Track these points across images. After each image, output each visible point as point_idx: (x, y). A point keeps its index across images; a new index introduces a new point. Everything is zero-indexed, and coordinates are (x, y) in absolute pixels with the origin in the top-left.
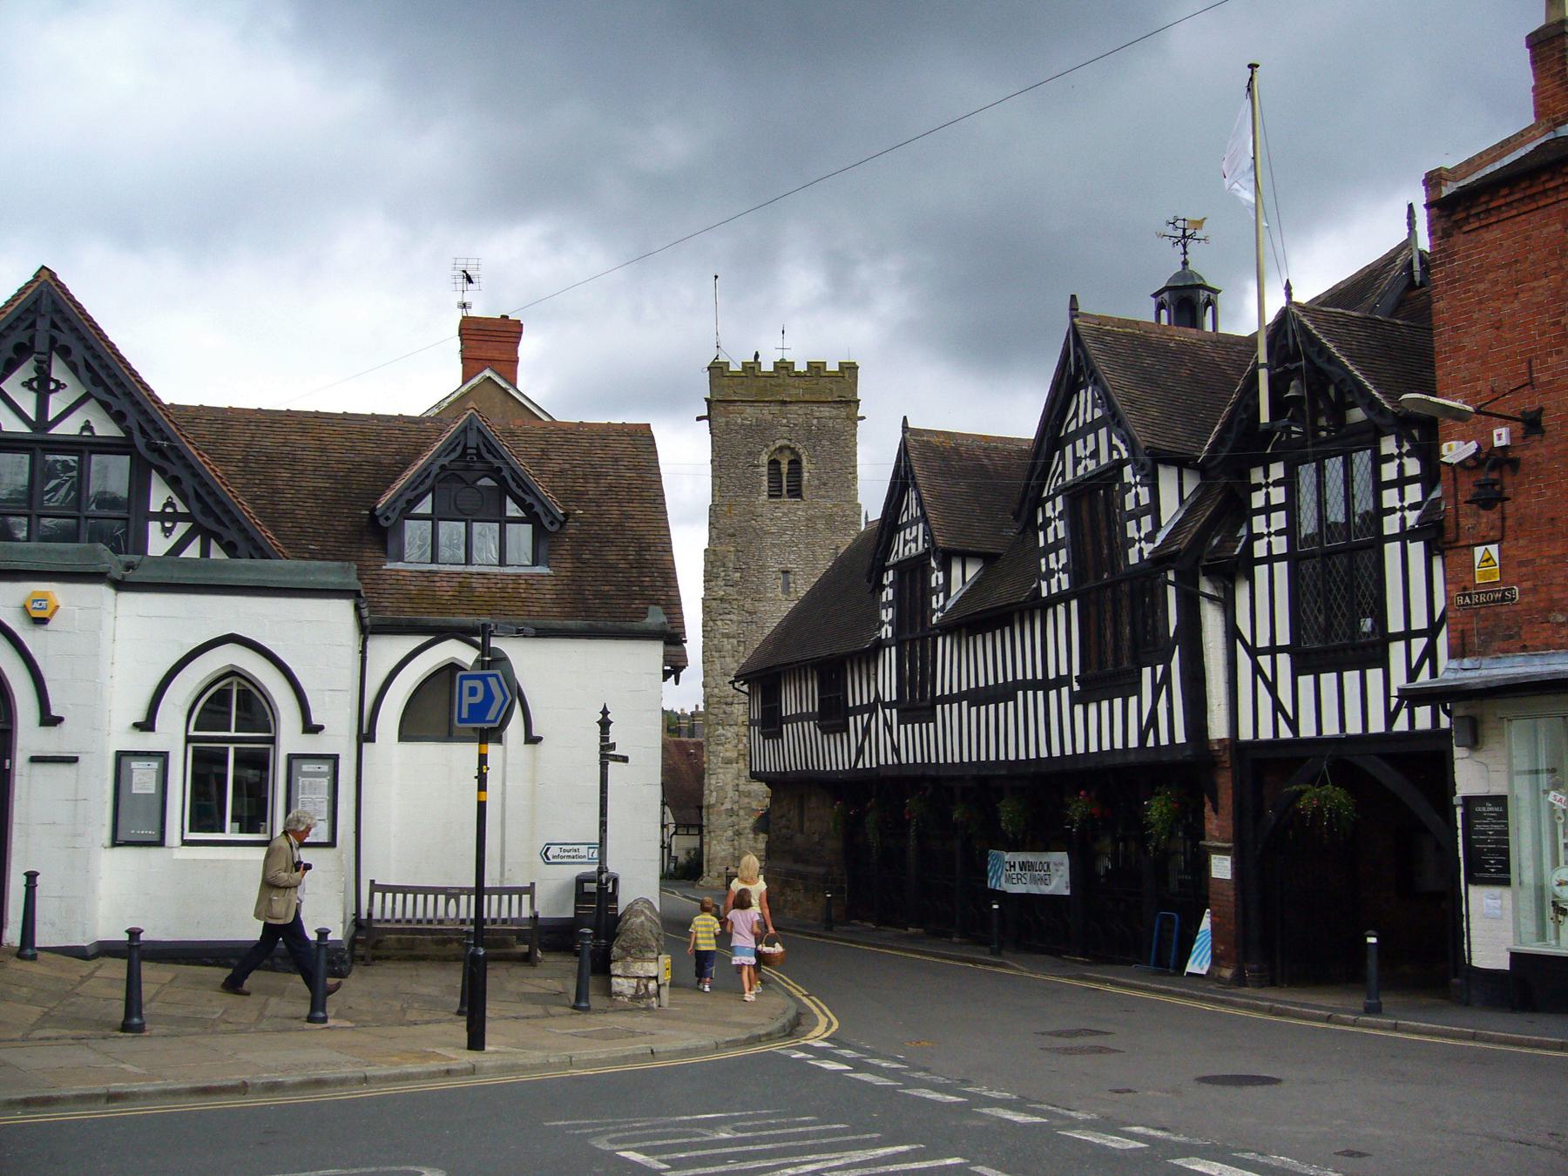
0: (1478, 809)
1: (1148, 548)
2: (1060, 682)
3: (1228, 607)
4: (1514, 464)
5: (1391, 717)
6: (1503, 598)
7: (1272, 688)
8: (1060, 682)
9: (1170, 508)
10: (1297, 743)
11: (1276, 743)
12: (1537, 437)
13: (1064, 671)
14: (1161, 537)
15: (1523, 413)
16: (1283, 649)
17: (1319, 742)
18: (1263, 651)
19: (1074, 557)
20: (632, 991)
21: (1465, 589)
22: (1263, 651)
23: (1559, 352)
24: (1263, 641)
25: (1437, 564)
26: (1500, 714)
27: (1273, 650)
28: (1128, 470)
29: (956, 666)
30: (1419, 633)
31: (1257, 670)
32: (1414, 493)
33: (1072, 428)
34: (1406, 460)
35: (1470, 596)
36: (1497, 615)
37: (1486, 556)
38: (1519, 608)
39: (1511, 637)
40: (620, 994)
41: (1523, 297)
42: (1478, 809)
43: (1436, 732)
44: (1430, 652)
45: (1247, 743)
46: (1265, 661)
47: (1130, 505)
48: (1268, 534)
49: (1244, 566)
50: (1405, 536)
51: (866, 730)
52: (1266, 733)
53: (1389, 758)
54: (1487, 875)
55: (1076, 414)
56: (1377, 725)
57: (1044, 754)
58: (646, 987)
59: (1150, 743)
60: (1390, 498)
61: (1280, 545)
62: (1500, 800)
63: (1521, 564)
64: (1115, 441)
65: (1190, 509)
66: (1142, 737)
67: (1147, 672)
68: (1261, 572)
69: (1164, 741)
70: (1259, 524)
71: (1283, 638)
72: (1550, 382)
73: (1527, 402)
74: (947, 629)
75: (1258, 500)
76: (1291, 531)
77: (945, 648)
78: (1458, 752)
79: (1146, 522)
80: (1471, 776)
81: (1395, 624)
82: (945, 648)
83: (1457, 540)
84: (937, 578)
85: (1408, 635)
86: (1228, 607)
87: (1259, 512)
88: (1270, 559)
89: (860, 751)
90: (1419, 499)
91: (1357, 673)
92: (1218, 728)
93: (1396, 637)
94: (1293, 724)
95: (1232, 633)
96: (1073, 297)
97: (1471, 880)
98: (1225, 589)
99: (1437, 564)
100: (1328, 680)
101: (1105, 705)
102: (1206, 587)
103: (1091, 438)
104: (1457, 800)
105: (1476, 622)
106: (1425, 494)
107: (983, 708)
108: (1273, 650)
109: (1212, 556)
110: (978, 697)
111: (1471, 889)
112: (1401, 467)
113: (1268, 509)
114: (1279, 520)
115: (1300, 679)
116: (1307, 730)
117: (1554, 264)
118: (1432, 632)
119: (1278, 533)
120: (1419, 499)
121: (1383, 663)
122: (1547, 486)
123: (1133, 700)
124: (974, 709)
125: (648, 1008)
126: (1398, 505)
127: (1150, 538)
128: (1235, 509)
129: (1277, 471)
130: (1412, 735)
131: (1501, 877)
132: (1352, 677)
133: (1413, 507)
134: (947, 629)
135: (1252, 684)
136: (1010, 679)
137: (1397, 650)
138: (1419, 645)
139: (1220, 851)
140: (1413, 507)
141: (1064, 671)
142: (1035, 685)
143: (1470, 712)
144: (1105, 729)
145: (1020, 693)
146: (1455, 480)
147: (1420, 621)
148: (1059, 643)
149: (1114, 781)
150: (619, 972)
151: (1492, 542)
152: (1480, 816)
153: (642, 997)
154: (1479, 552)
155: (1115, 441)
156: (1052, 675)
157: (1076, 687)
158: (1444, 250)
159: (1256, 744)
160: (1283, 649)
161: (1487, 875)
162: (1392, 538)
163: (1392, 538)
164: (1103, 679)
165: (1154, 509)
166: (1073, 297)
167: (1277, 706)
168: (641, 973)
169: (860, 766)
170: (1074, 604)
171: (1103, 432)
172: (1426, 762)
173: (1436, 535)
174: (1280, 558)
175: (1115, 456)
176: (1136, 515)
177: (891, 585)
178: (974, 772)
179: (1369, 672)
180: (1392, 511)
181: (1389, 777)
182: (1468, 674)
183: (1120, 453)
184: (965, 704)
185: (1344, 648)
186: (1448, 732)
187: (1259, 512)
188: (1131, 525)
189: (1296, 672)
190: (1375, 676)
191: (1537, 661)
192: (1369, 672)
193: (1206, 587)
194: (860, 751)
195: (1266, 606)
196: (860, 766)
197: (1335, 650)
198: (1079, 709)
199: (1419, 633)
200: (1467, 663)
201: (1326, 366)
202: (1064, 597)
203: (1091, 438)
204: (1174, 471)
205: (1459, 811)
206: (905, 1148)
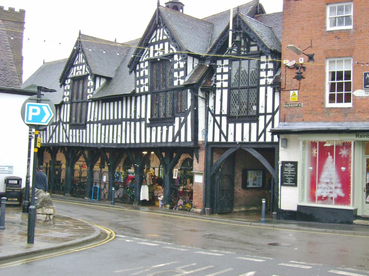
0: (286, 165)
1: (182, 82)
2: (141, 120)
3: (207, 101)
4: (304, 68)
5: (258, 137)
6: (298, 106)
7: (220, 127)
8: (141, 120)
9: (190, 70)
10: (227, 143)
11: (220, 143)
12: (312, 62)
13: (143, 116)
14: (187, 78)
15: (308, 54)
16: (224, 115)
17: (235, 143)
18: (217, 115)
19: (151, 81)
20: (45, 219)
21: (286, 102)
22: (217, 115)
23: (320, 39)
24: (218, 112)
25: (277, 95)
26: (299, 139)
27: (221, 115)
28: (176, 57)
29: (93, 112)
30: (269, 114)
31: (215, 121)
32: (270, 73)
33: (154, 41)
34: (269, 64)
35: (288, 104)
36: (296, 111)
37: (293, 95)
38: (302, 109)
39: (299, 117)
40: (40, 220)
41: (311, 22)
42: (286, 165)
43: (272, 143)
44: (272, 119)
45: (210, 142)
46: (218, 119)
47: (89, 85)
48: (221, 80)
49: (214, 90)
50: (266, 85)
51: (54, 131)
52: (217, 140)
53: (257, 150)
54: (287, 183)
55: (156, 37)
56: (254, 139)
57: (133, 141)
58: (49, 217)
59: (177, 140)
60: (226, 70)
61: (226, 84)
62: (295, 164)
63: (304, 97)
64: (171, 47)
65: (196, 71)
66: (174, 139)
67: (177, 119)
68: (218, 92)
69: (183, 140)
70: (219, 77)
71: (225, 112)
72: (317, 47)
73: (310, 52)
74: (93, 100)
75: (219, 70)
76: (229, 80)
77: (92, 106)
78: (281, 149)
79: (182, 73)
80: (284, 155)
81: (262, 111)
82: (92, 106)
83: (285, 88)
84: (90, 83)
85: (265, 114)
86: (207, 101)
87: (219, 74)
88: (222, 88)
89: (51, 137)
90: (272, 75)
91: (241, 124)
92: (201, 138)
93: (262, 114)
94: (226, 138)
95: (208, 110)
96: (80, 30)
97: (282, 184)
98: (206, 95)
99: (277, 95)
100: (239, 126)
101: (165, 128)
102: (200, 94)
103: (161, 45)
104: (280, 161)
105: (286, 111)
106: (274, 74)
107: (107, 126)
108: (221, 115)
109: (204, 84)
110: (105, 123)
111: (282, 187)
112: (267, 65)
113: (222, 73)
114: (226, 77)
115: (230, 125)
116: (231, 139)
117: (321, 14)
118: (273, 114)
119: (225, 81)
120: (272, 75)
121: (257, 121)
122: (314, 76)
123: (171, 128)
124: (103, 127)
125: (50, 224)
126: (265, 76)
127: (183, 78)
128: (211, 71)
129: (226, 62)
130: (265, 143)
131: (294, 183)
132: (246, 125)
133: (270, 77)
134: (93, 100)
135: (213, 125)
136: (120, 117)
137: (261, 119)
138: (269, 117)
139: (198, 174)
140: (270, 77)
141: (143, 116)
142: (131, 120)
143: (286, 137)
144: (162, 135)
145: (124, 123)
146: (286, 71)
147: (270, 110)
148: (144, 108)
149: (170, 153)
150: (40, 212)
151: (296, 90)
152: (287, 167)
153: (48, 221)
154: (292, 92)
155: (87, 69)
156: (128, 117)
157: (148, 122)
158: (288, 5)
159: (213, 143)
160: (224, 115)
161: (287, 183)
162: (263, 86)
163: (263, 86)
164: (155, 121)
165: (185, 69)
166: (80, 30)
167: (221, 132)
168: (48, 213)
169: (51, 142)
170: (149, 96)
171: (167, 44)
172: (270, 151)
173: (277, 86)
174: (225, 88)
175: (171, 51)
176: (178, 70)
177: (69, 84)
178: (102, 146)
179: (252, 124)
180: (263, 78)
181: (256, 155)
182: (286, 126)
183: (173, 50)
184: (100, 124)
185: (245, 117)
186: (277, 143)
187: (219, 74)
188: (89, 90)
189: (228, 122)
190: (254, 125)
191: (307, 124)
192: (252, 124)
193: (200, 94)
194: (51, 137)
195: (220, 101)
196: (51, 142)
197: (242, 117)
198: (148, 130)
199: (269, 114)
200: (286, 123)
201: (249, 33)
202: (146, 94)
203: (161, 45)
204: (192, 58)
205: (280, 165)
206: (304, 263)
